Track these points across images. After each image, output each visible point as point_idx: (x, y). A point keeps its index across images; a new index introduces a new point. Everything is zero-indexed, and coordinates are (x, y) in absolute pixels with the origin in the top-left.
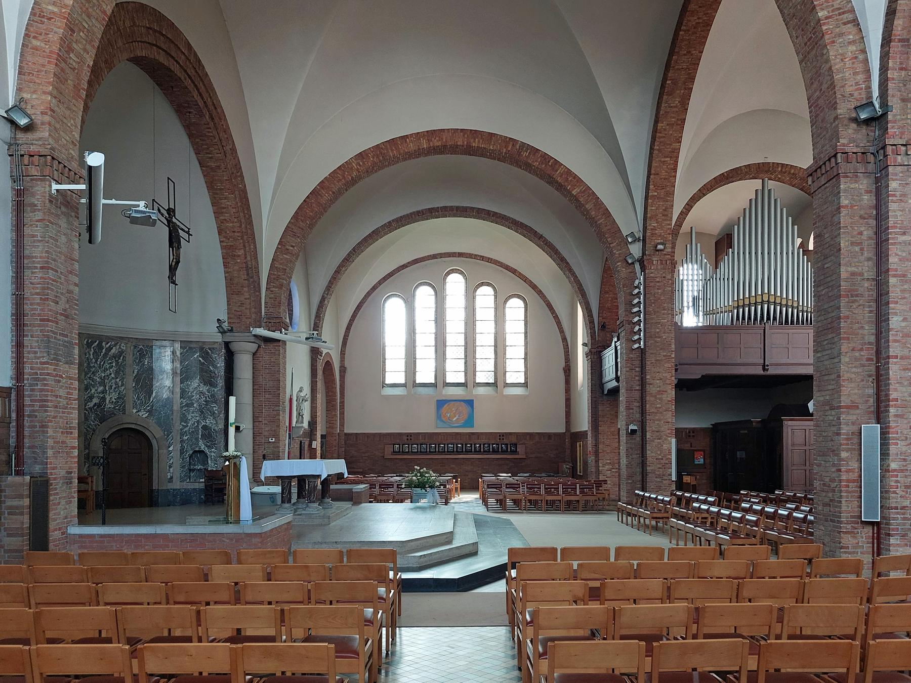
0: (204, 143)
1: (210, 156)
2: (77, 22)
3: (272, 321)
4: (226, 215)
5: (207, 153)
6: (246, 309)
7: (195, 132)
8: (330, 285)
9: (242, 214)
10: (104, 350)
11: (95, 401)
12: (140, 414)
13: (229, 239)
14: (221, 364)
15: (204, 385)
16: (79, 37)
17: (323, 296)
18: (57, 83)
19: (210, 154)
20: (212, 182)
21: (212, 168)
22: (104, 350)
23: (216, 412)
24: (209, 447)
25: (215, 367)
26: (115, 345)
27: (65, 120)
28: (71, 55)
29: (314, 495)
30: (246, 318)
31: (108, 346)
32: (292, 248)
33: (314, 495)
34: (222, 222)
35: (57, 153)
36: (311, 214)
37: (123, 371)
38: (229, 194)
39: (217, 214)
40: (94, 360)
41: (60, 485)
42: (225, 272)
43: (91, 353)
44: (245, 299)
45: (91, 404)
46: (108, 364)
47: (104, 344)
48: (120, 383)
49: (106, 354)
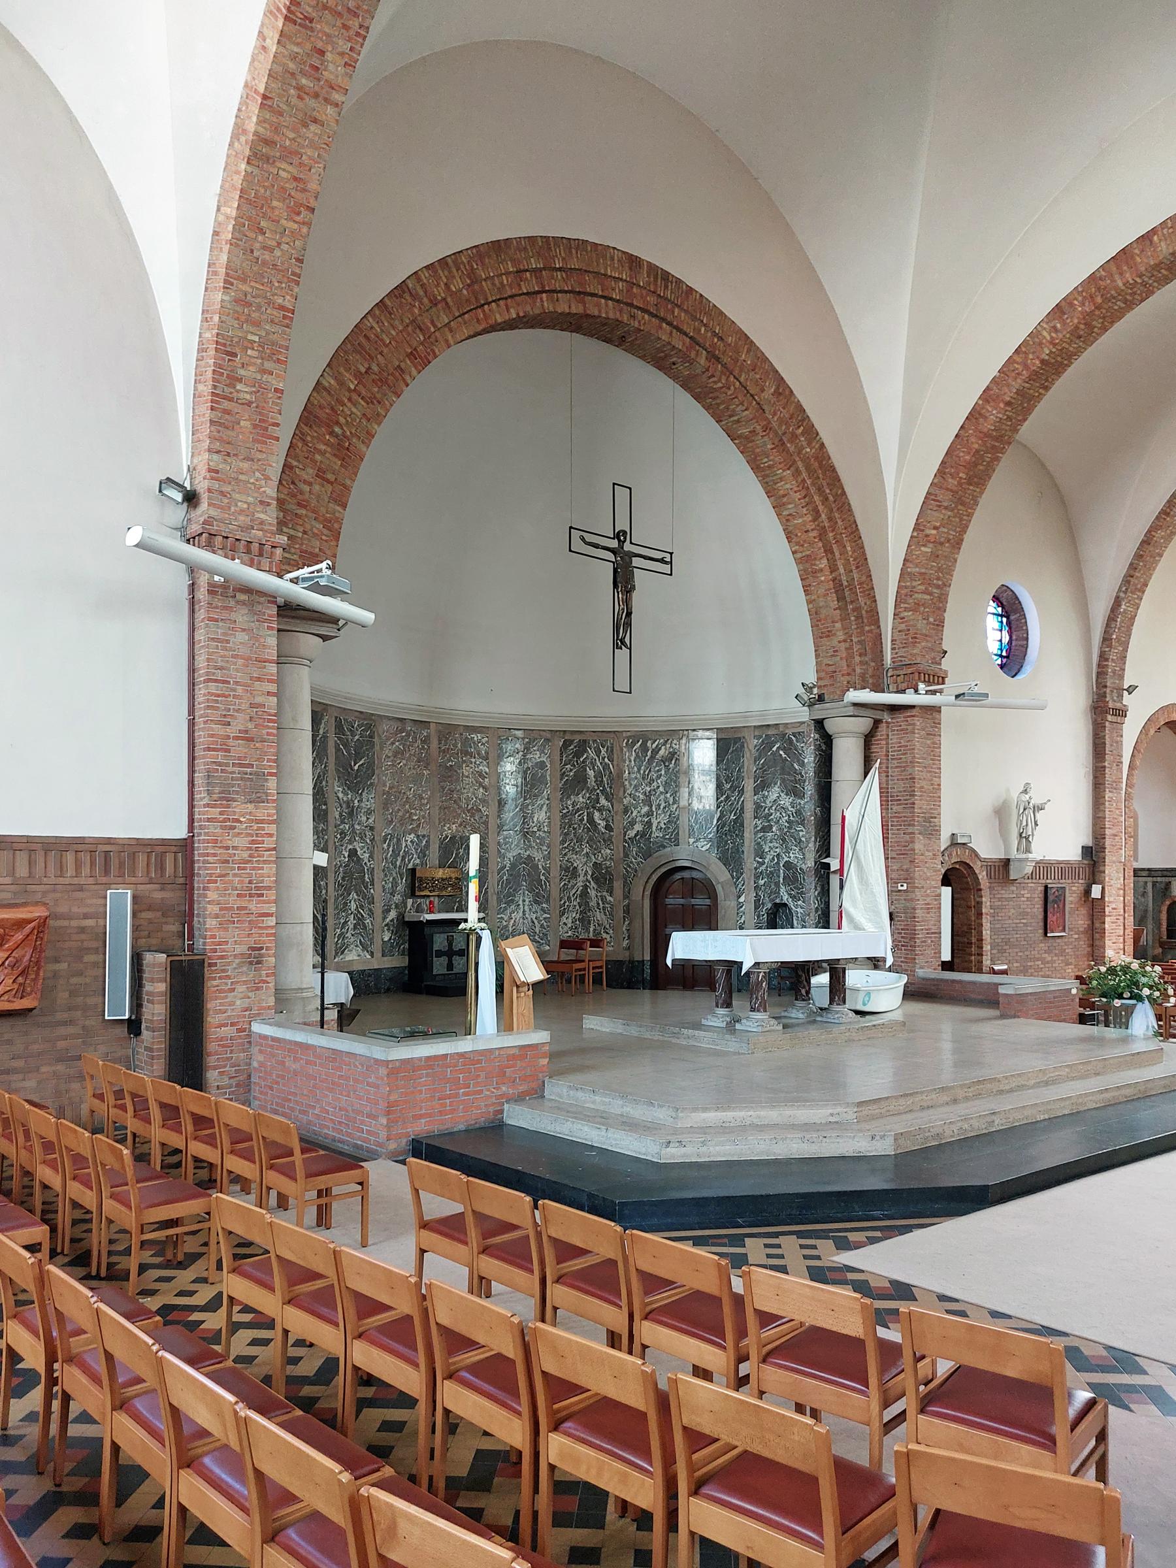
0: (718, 401)
1: (735, 418)
2: (236, 340)
3: (901, 672)
4: (790, 506)
5: (730, 416)
6: (841, 659)
7: (699, 390)
8: (1132, 572)
9: (816, 498)
10: (649, 753)
11: (638, 827)
12: (699, 844)
13: (802, 546)
14: (810, 758)
15: (787, 795)
16: (248, 358)
17: (1117, 597)
18: (219, 432)
19: (733, 416)
20: (755, 459)
21: (746, 438)
22: (649, 753)
23: (803, 839)
24: (793, 897)
25: (802, 764)
26: (665, 744)
27: (242, 477)
28: (238, 387)
29: (757, 998)
30: (843, 675)
31: (654, 746)
32: (934, 532)
33: (757, 998)
34: (787, 520)
35: (217, 526)
36: (968, 458)
37: (675, 782)
38: (784, 471)
39: (778, 507)
40: (636, 769)
41: (234, 965)
42: (809, 602)
43: (632, 759)
44: (840, 642)
45: (632, 833)
46: (655, 772)
47: (649, 744)
48: (671, 801)
49: (653, 757)
